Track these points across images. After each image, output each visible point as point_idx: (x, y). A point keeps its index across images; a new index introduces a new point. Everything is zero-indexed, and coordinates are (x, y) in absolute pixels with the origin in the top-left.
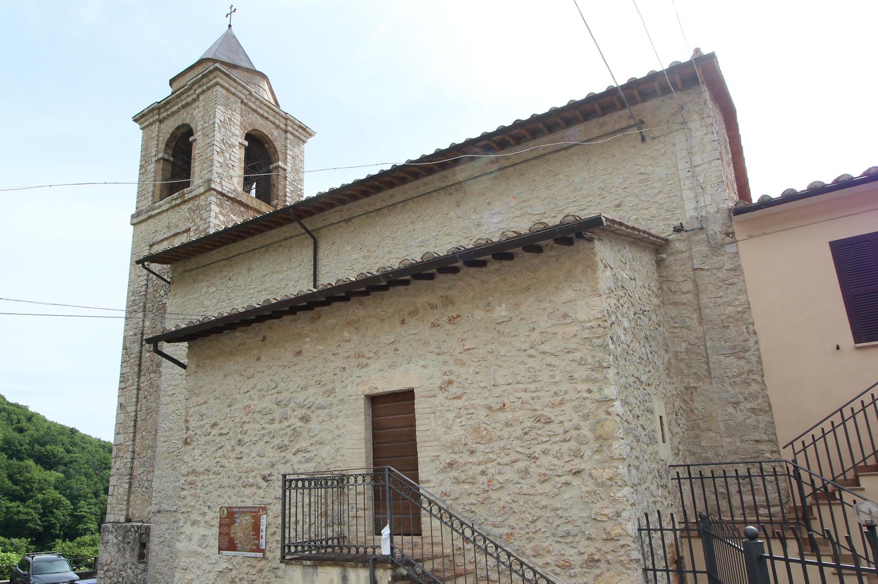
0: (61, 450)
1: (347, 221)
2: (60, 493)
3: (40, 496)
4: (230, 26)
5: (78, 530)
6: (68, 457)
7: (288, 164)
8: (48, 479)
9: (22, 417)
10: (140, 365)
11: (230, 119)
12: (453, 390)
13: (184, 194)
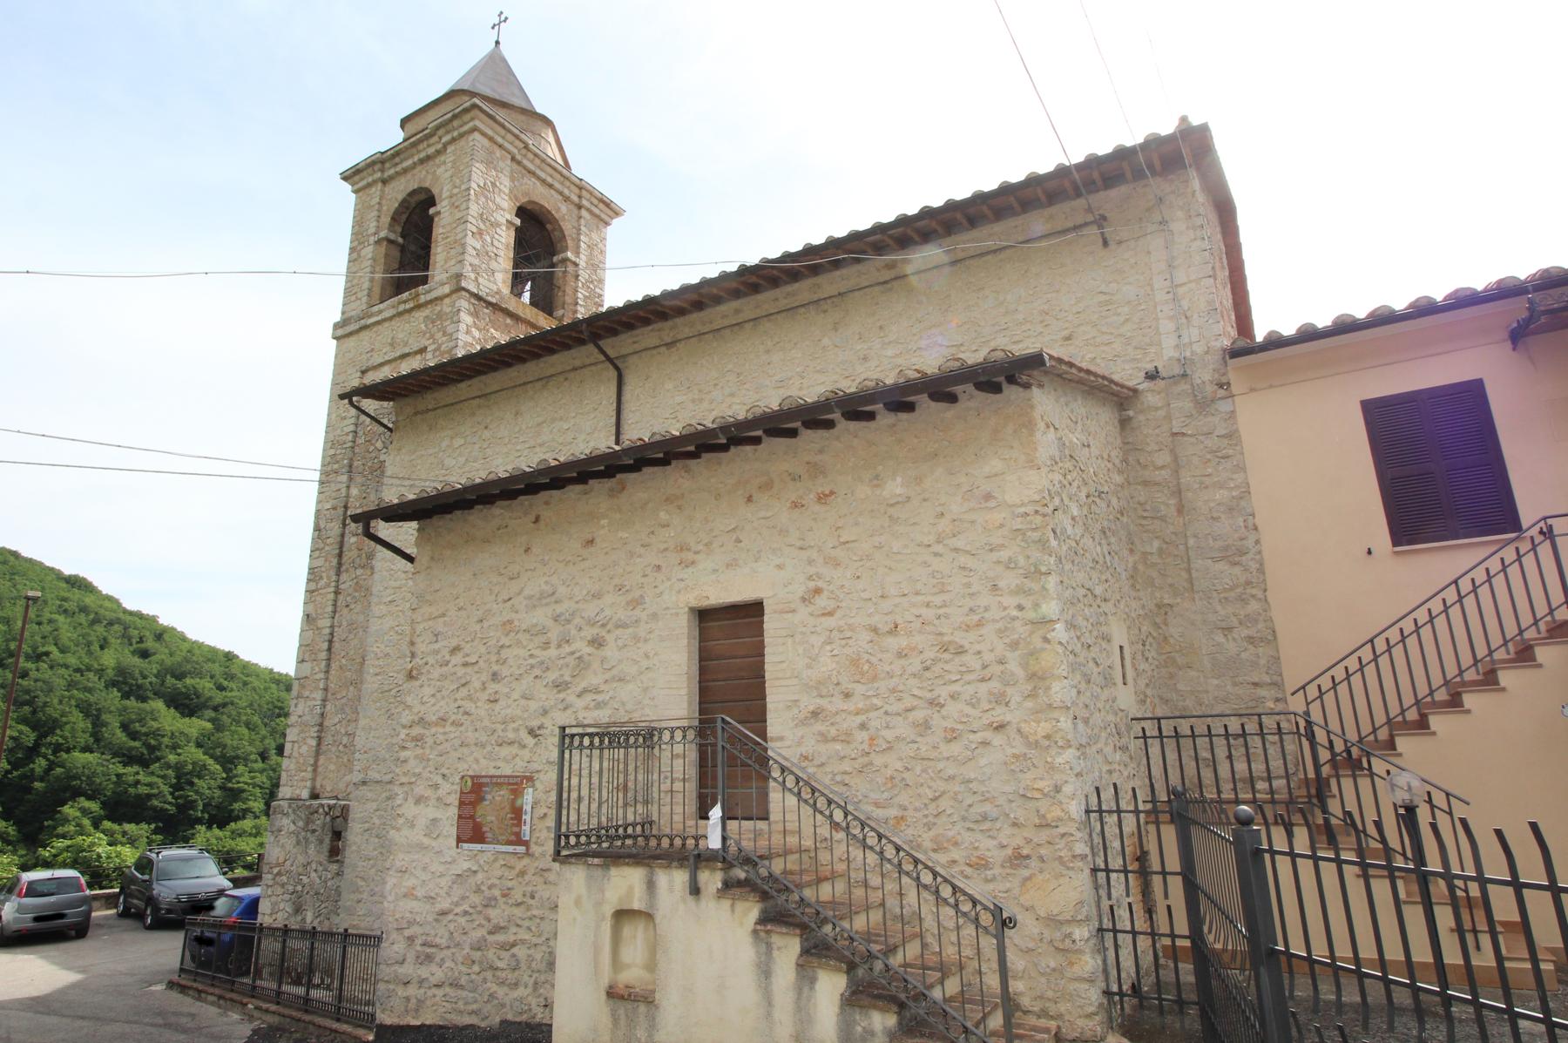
2: (205, 753)
4: (497, 43)
6: (219, 697)
10: (340, 555)
11: (494, 184)
12: (822, 602)
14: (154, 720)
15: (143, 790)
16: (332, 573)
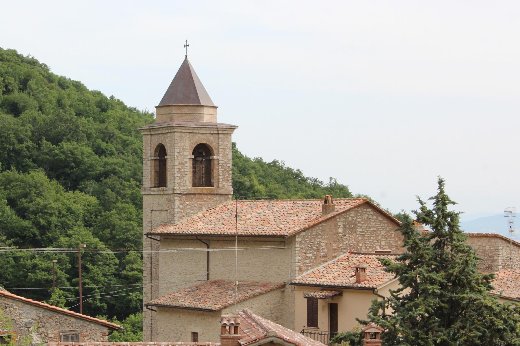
0: (88, 150)
1: (218, 241)
2: (95, 234)
3: (63, 239)
4: (186, 56)
5: (130, 301)
6: (99, 163)
7: (221, 155)
8: (74, 207)
9: (12, 80)
10: (151, 274)
11: (183, 148)
12: (204, 335)
13: (163, 191)
14: (39, 195)
15: (42, 275)
16: (150, 279)
